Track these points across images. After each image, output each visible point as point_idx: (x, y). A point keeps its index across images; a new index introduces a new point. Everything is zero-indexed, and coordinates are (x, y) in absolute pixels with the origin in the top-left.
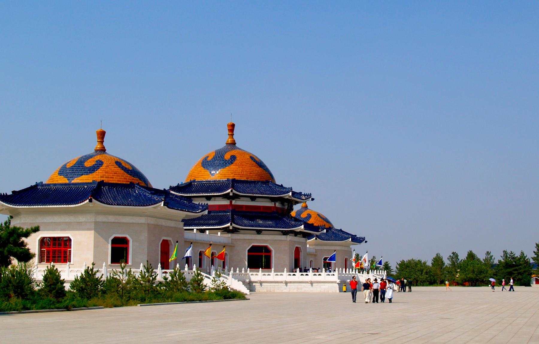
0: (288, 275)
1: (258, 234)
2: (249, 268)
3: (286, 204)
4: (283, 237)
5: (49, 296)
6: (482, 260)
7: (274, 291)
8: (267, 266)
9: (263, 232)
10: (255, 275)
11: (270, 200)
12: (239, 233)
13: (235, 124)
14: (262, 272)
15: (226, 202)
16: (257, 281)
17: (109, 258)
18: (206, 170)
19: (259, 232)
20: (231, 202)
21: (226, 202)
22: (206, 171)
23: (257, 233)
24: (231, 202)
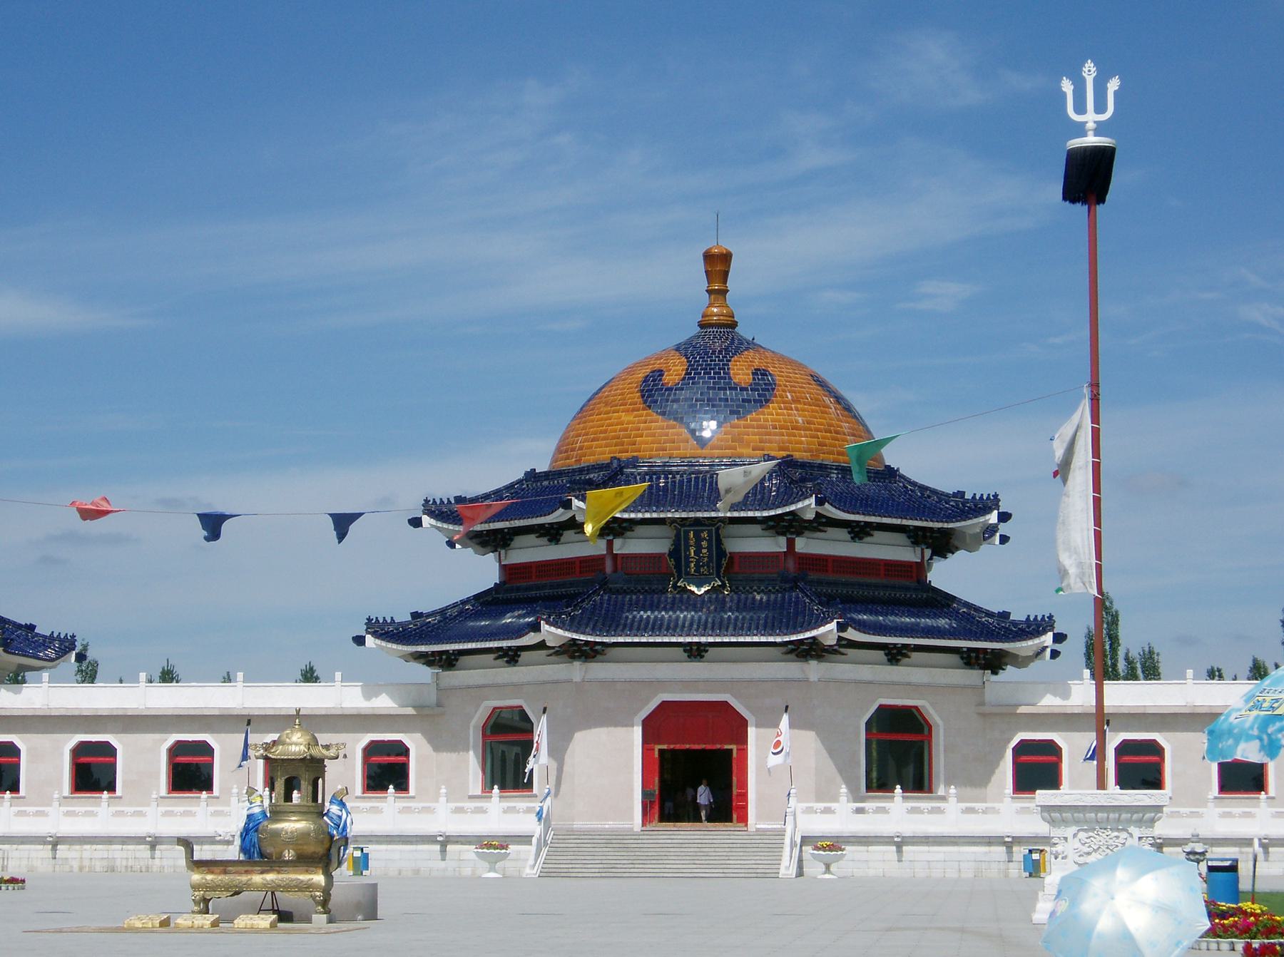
0: (113, 815)
1: (892, 665)
2: (496, 787)
3: (555, 532)
4: (793, 669)
5: (1057, 851)
6: (94, 777)
7: (460, 874)
8: (919, 783)
9: (712, 650)
10: (472, 812)
11: (909, 537)
12: (839, 657)
13: (733, 252)
14: (960, 799)
15: (776, 545)
16: (436, 836)
17: (377, 736)
18: (672, 422)
19: (895, 655)
20: (791, 544)
21: (776, 545)
22: (674, 427)
23: (889, 660)
24: (791, 544)
